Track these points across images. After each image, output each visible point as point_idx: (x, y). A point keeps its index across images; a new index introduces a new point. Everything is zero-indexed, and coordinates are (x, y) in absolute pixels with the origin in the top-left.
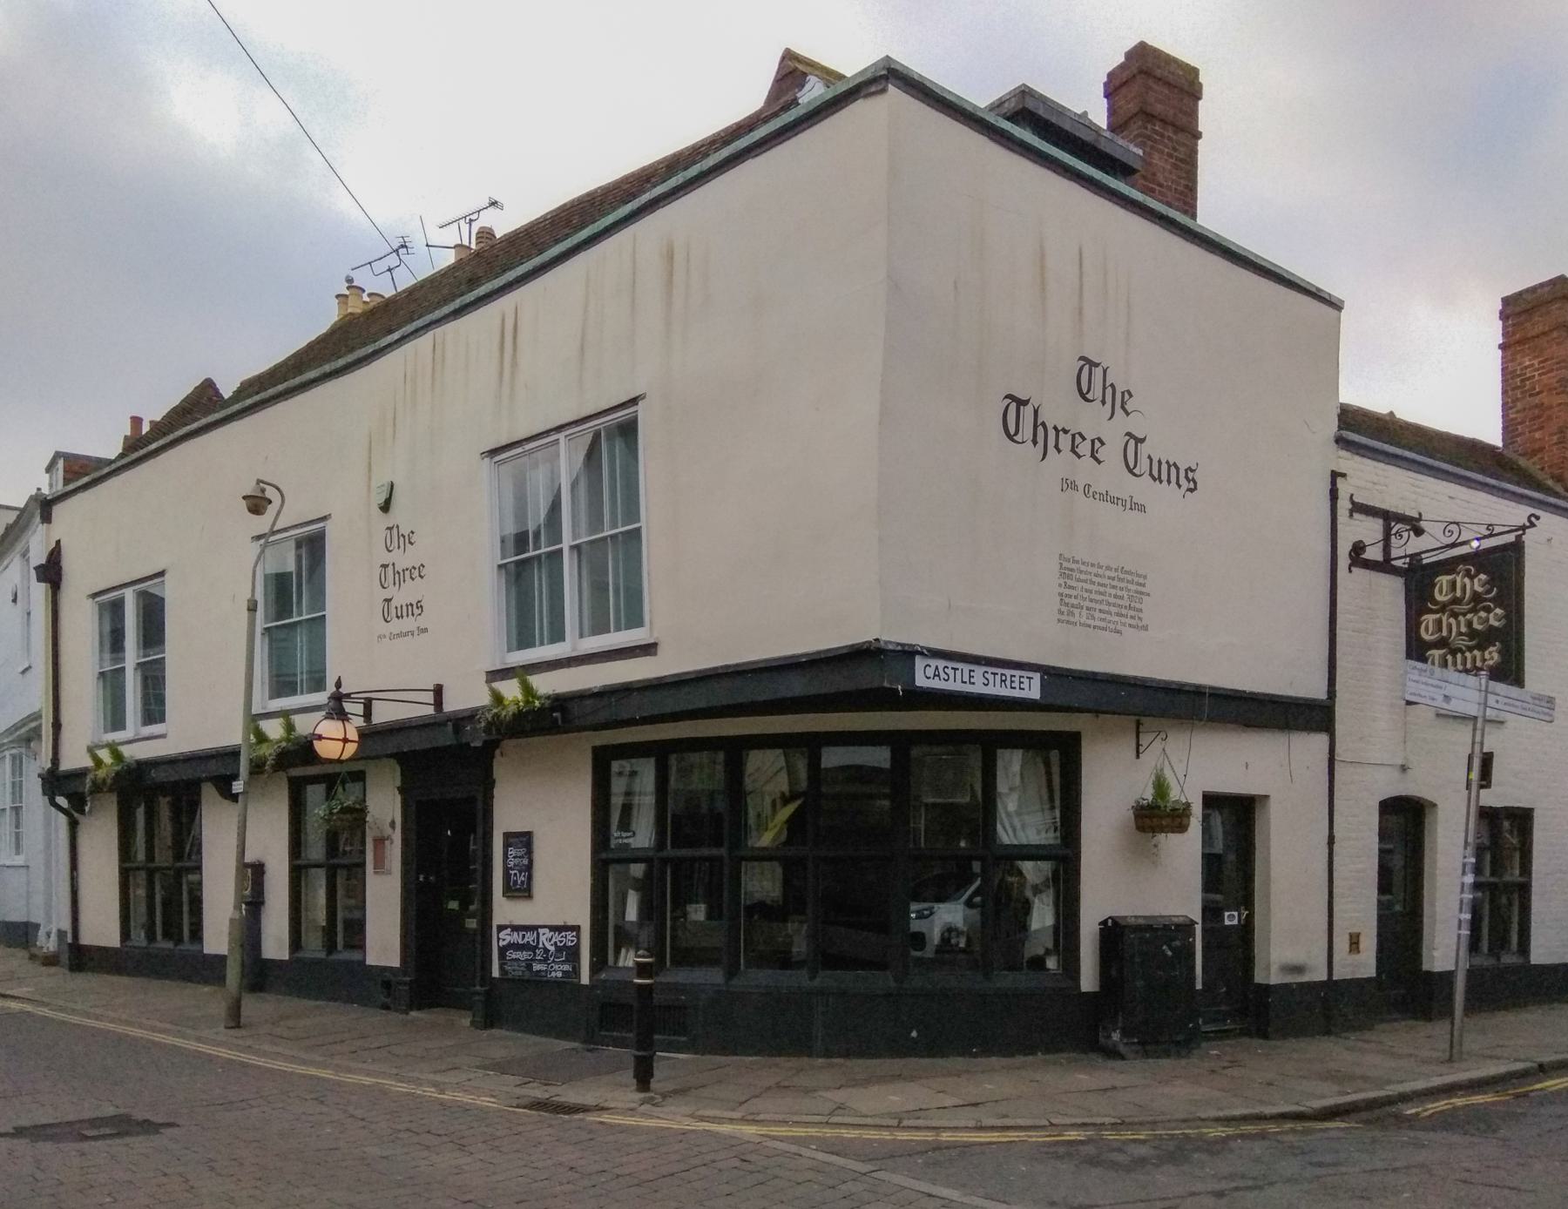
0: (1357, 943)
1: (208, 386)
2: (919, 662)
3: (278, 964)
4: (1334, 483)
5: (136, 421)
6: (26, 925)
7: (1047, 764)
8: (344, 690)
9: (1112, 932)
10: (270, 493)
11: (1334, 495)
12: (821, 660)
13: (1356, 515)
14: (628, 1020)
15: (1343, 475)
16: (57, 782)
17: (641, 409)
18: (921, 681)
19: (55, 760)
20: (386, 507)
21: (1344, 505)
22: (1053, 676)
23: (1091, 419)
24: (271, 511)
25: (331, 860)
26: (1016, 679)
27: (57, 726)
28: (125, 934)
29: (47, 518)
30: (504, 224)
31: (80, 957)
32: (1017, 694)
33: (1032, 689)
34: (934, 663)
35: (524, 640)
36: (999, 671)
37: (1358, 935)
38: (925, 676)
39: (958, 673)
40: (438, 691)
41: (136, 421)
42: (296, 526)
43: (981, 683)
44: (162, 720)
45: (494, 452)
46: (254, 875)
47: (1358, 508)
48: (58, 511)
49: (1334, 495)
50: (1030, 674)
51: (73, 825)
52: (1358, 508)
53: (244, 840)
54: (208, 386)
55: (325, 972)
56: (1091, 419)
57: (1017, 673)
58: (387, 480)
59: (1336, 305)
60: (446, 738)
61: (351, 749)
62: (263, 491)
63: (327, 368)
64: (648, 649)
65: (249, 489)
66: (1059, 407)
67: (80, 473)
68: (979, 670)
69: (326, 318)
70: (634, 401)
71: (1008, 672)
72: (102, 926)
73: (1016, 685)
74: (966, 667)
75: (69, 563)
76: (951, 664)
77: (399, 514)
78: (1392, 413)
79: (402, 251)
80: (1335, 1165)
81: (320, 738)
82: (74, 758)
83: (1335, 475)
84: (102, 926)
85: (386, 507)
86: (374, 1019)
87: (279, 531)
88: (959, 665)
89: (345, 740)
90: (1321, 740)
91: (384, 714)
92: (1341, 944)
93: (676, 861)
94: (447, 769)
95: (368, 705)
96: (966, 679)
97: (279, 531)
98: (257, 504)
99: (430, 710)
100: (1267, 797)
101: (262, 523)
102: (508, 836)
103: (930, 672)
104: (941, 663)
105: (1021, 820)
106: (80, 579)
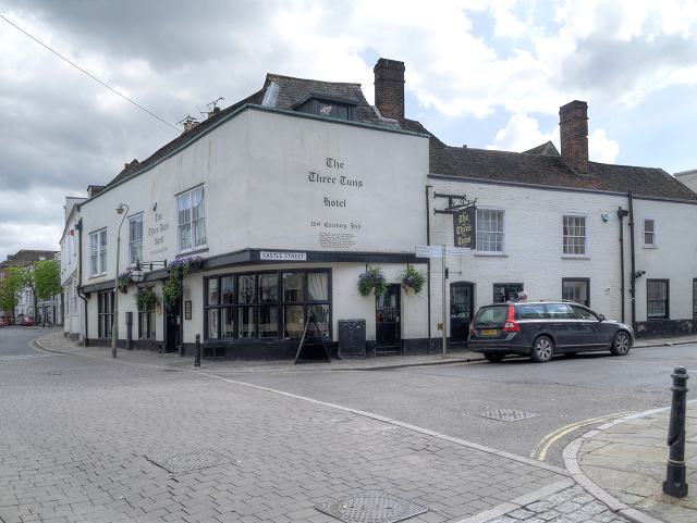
2: (262, 253)
7: (71, 326)
9: (341, 323)
14: (213, 352)
16: (80, 289)
21: (431, 195)
22: (308, 253)
23: (333, 172)
27: (81, 272)
29: (79, 211)
30: (223, 106)
31: (88, 343)
35: (182, 249)
38: (263, 256)
43: (284, 257)
45: (176, 195)
46: (130, 315)
47: (436, 195)
48: (82, 208)
51: (86, 302)
53: (127, 304)
55: (143, 344)
56: (333, 172)
61: (141, 279)
64: (206, 250)
65: (117, 206)
66: (323, 170)
67: (96, 191)
69: (181, 130)
72: (93, 334)
75: (84, 223)
78: (465, 146)
80: (509, 383)
82: (85, 282)
83: (427, 187)
84: (93, 334)
86: (157, 354)
91: (155, 268)
93: (229, 305)
95: (151, 265)
98: (120, 211)
99: (163, 267)
101: (122, 216)
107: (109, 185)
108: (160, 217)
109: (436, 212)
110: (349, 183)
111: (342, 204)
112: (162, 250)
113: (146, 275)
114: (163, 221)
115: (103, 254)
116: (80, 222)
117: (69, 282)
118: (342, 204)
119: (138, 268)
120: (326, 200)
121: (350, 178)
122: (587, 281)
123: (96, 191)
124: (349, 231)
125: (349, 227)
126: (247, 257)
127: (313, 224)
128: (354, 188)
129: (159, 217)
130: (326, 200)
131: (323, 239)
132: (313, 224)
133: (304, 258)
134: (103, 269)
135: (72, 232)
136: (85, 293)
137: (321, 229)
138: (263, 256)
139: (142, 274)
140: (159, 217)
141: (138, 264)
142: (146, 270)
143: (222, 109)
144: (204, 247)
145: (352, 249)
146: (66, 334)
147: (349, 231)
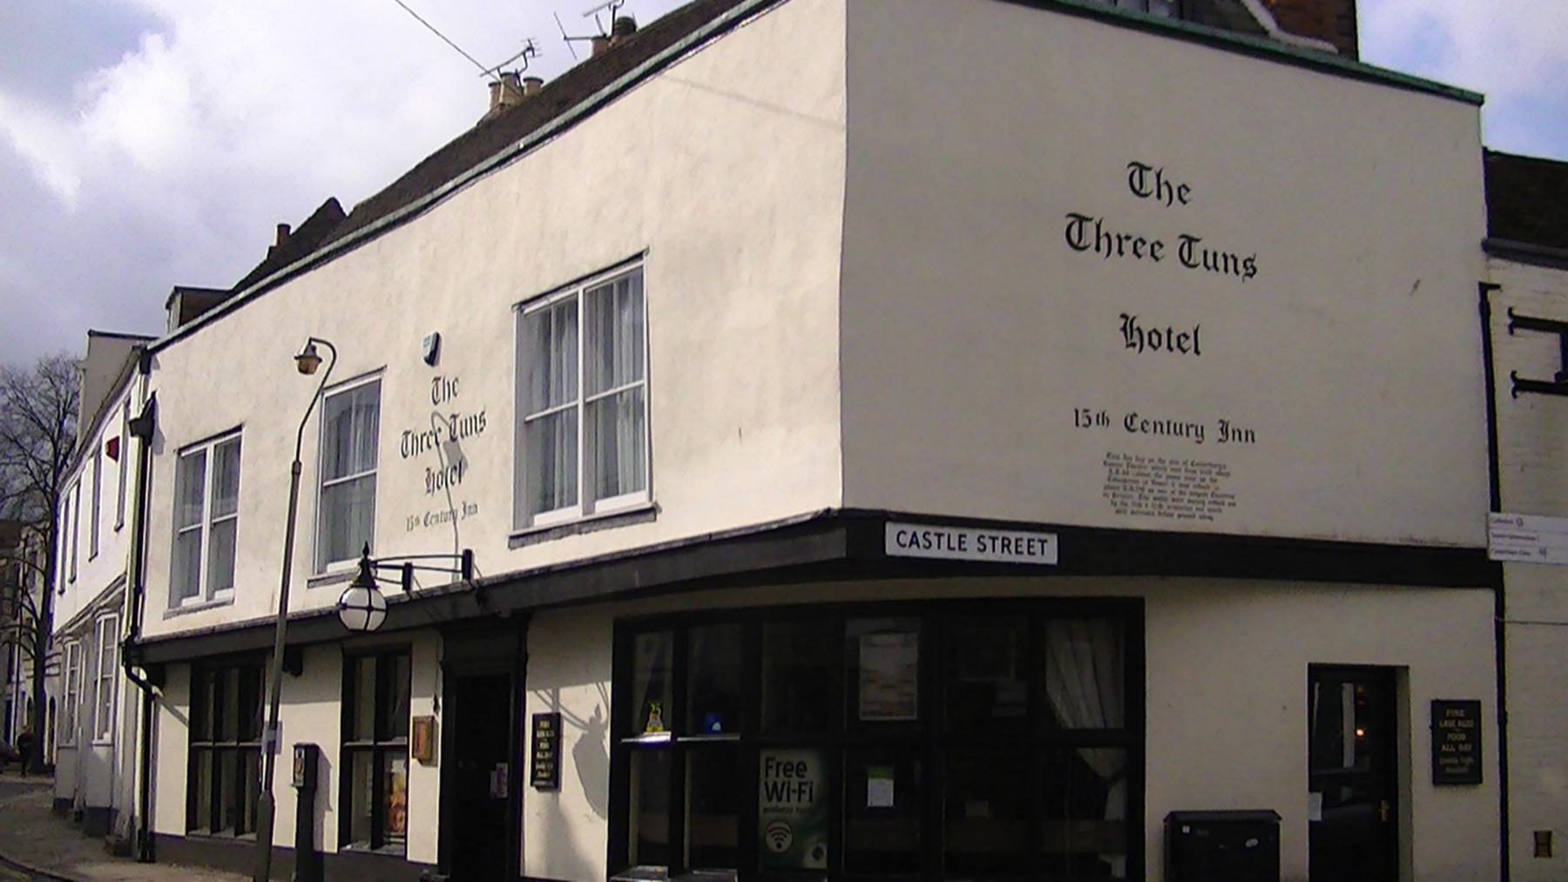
0: (1537, 844)
1: (332, 204)
2: (891, 530)
3: (332, 855)
4: (1483, 296)
5: (284, 229)
6: (109, 810)
8: (371, 558)
10: (322, 351)
11: (1485, 310)
12: (660, 552)
13: (1517, 331)
15: (1497, 287)
16: (135, 651)
17: (385, 374)
18: (892, 548)
19: (135, 630)
20: (432, 359)
21: (1500, 321)
22: (1068, 535)
24: (322, 369)
25: (374, 739)
26: (1025, 543)
28: (191, 824)
29: (146, 371)
32: (1025, 558)
33: (1049, 553)
34: (910, 529)
36: (1001, 534)
37: (1549, 834)
38: (896, 542)
39: (944, 540)
40: (468, 557)
41: (284, 229)
42: (354, 379)
43: (973, 549)
44: (230, 585)
46: (310, 756)
47: (1519, 322)
49: (1485, 310)
50: (1044, 536)
51: (149, 698)
52: (1519, 322)
54: (332, 204)
57: (1026, 535)
58: (432, 333)
59: (1477, 100)
60: (470, 608)
61: (377, 619)
62: (314, 349)
63: (390, 217)
64: (650, 513)
66: (1121, 212)
67: (197, 307)
68: (972, 535)
70: (639, 256)
71: (1013, 536)
73: (1024, 549)
74: (954, 533)
76: (932, 530)
77: (445, 365)
79: (529, 54)
81: (345, 607)
82: (155, 626)
83: (1484, 288)
85: (432, 359)
87: (330, 387)
88: (945, 530)
89: (370, 609)
90: (1486, 598)
91: (425, 581)
92: (1522, 844)
94: (482, 639)
95: (408, 570)
96: (954, 543)
97: (330, 387)
98: (307, 362)
100: (1407, 668)
101: (313, 381)
102: (1439, 708)
103: (905, 539)
104: (920, 530)
105: (1077, 697)
106: (173, 428)
107: (243, 285)
108: (452, 390)
109: (1521, 386)
110: (1212, 262)
111: (1184, 342)
112: (455, 524)
113: (392, 605)
114: (464, 405)
115: (225, 531)
116: (150, 408)
117: (85, 625)
118: (1184, 342)
119: (366, 580)
120: (1128, 325)
121: (1211, 242)
122: (1479, 703)
123: (197, 307)
124: (1211, 450)
125: (1213, 433)
126: (834, 547)
127: (1084, 418)
128: (1228, 282)
129: (444, 389)
130: (1128, 325)
131: (1120, 476)
132: (1084, 418)
133: (1049, 553)
134: (224, 577)
135: (114, 448)
136: (154, 662)
137: (1112, 438)
138: (896, 542)
139: (379, 603)
140: (444, 389)
141: (366, 565)
142: (389, 587)
143: (641, 23)
144: (637, 500)
145: (1227, 523)
146: (62, 806)
147: (1211, 450)
